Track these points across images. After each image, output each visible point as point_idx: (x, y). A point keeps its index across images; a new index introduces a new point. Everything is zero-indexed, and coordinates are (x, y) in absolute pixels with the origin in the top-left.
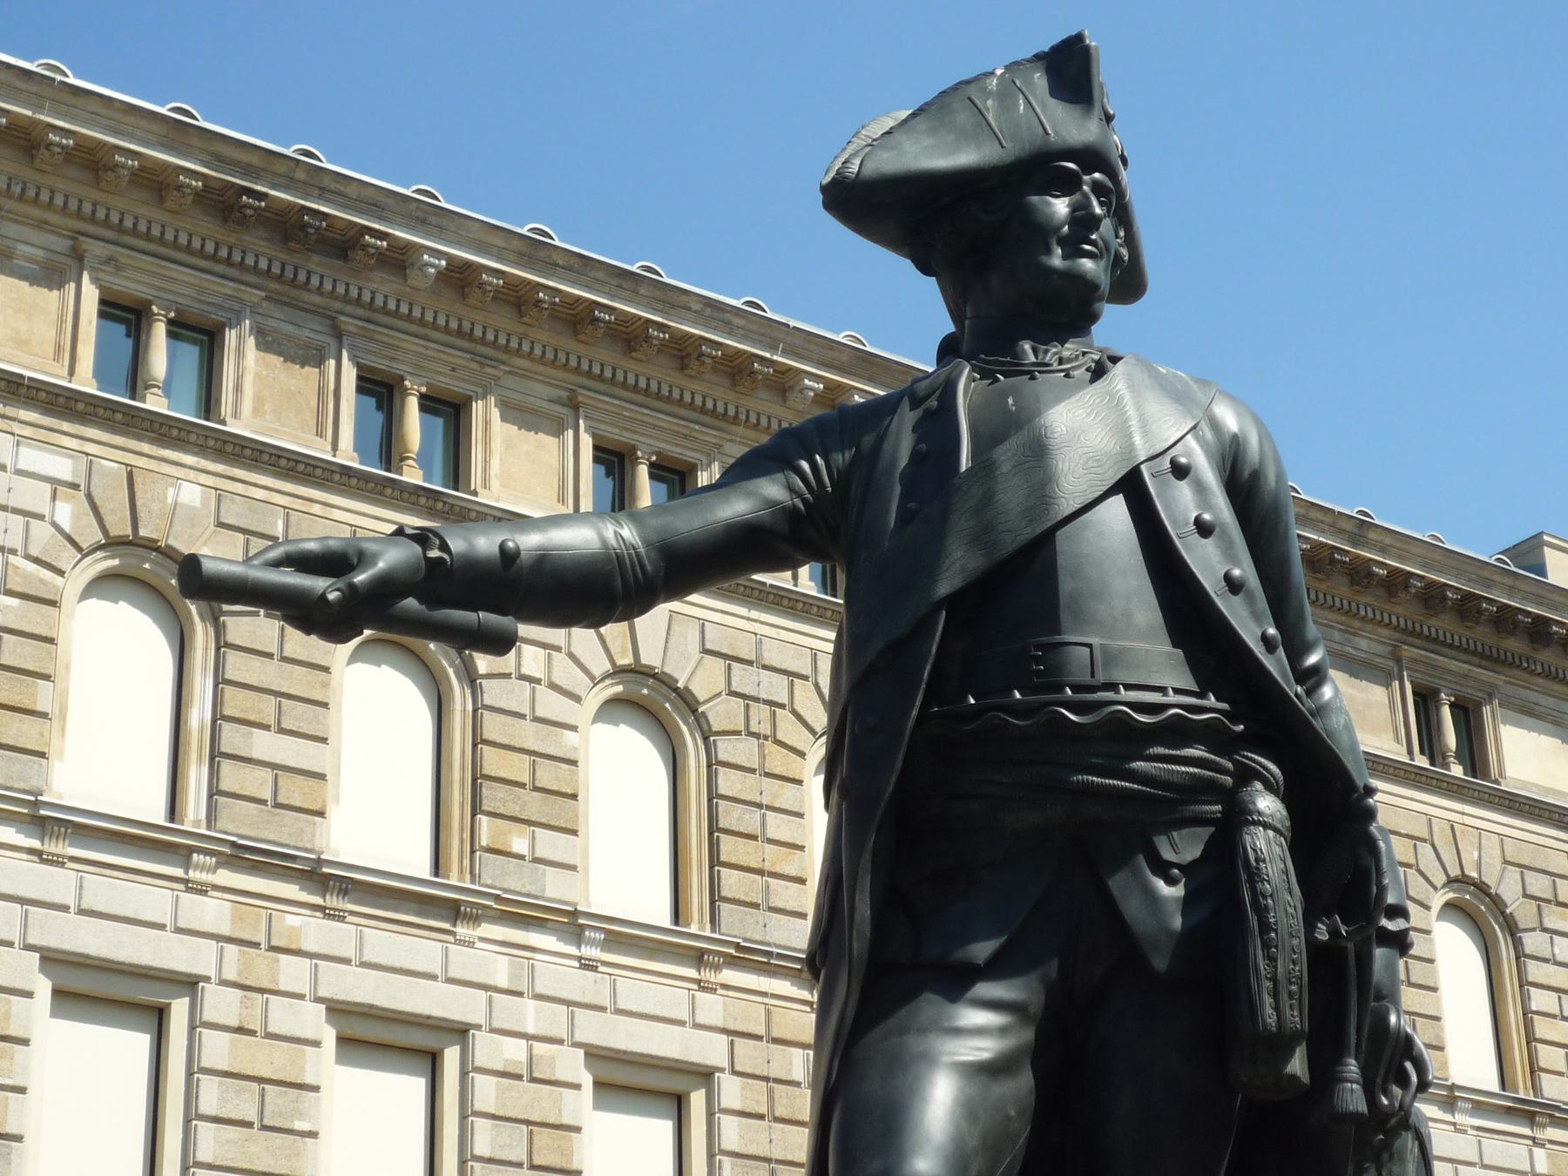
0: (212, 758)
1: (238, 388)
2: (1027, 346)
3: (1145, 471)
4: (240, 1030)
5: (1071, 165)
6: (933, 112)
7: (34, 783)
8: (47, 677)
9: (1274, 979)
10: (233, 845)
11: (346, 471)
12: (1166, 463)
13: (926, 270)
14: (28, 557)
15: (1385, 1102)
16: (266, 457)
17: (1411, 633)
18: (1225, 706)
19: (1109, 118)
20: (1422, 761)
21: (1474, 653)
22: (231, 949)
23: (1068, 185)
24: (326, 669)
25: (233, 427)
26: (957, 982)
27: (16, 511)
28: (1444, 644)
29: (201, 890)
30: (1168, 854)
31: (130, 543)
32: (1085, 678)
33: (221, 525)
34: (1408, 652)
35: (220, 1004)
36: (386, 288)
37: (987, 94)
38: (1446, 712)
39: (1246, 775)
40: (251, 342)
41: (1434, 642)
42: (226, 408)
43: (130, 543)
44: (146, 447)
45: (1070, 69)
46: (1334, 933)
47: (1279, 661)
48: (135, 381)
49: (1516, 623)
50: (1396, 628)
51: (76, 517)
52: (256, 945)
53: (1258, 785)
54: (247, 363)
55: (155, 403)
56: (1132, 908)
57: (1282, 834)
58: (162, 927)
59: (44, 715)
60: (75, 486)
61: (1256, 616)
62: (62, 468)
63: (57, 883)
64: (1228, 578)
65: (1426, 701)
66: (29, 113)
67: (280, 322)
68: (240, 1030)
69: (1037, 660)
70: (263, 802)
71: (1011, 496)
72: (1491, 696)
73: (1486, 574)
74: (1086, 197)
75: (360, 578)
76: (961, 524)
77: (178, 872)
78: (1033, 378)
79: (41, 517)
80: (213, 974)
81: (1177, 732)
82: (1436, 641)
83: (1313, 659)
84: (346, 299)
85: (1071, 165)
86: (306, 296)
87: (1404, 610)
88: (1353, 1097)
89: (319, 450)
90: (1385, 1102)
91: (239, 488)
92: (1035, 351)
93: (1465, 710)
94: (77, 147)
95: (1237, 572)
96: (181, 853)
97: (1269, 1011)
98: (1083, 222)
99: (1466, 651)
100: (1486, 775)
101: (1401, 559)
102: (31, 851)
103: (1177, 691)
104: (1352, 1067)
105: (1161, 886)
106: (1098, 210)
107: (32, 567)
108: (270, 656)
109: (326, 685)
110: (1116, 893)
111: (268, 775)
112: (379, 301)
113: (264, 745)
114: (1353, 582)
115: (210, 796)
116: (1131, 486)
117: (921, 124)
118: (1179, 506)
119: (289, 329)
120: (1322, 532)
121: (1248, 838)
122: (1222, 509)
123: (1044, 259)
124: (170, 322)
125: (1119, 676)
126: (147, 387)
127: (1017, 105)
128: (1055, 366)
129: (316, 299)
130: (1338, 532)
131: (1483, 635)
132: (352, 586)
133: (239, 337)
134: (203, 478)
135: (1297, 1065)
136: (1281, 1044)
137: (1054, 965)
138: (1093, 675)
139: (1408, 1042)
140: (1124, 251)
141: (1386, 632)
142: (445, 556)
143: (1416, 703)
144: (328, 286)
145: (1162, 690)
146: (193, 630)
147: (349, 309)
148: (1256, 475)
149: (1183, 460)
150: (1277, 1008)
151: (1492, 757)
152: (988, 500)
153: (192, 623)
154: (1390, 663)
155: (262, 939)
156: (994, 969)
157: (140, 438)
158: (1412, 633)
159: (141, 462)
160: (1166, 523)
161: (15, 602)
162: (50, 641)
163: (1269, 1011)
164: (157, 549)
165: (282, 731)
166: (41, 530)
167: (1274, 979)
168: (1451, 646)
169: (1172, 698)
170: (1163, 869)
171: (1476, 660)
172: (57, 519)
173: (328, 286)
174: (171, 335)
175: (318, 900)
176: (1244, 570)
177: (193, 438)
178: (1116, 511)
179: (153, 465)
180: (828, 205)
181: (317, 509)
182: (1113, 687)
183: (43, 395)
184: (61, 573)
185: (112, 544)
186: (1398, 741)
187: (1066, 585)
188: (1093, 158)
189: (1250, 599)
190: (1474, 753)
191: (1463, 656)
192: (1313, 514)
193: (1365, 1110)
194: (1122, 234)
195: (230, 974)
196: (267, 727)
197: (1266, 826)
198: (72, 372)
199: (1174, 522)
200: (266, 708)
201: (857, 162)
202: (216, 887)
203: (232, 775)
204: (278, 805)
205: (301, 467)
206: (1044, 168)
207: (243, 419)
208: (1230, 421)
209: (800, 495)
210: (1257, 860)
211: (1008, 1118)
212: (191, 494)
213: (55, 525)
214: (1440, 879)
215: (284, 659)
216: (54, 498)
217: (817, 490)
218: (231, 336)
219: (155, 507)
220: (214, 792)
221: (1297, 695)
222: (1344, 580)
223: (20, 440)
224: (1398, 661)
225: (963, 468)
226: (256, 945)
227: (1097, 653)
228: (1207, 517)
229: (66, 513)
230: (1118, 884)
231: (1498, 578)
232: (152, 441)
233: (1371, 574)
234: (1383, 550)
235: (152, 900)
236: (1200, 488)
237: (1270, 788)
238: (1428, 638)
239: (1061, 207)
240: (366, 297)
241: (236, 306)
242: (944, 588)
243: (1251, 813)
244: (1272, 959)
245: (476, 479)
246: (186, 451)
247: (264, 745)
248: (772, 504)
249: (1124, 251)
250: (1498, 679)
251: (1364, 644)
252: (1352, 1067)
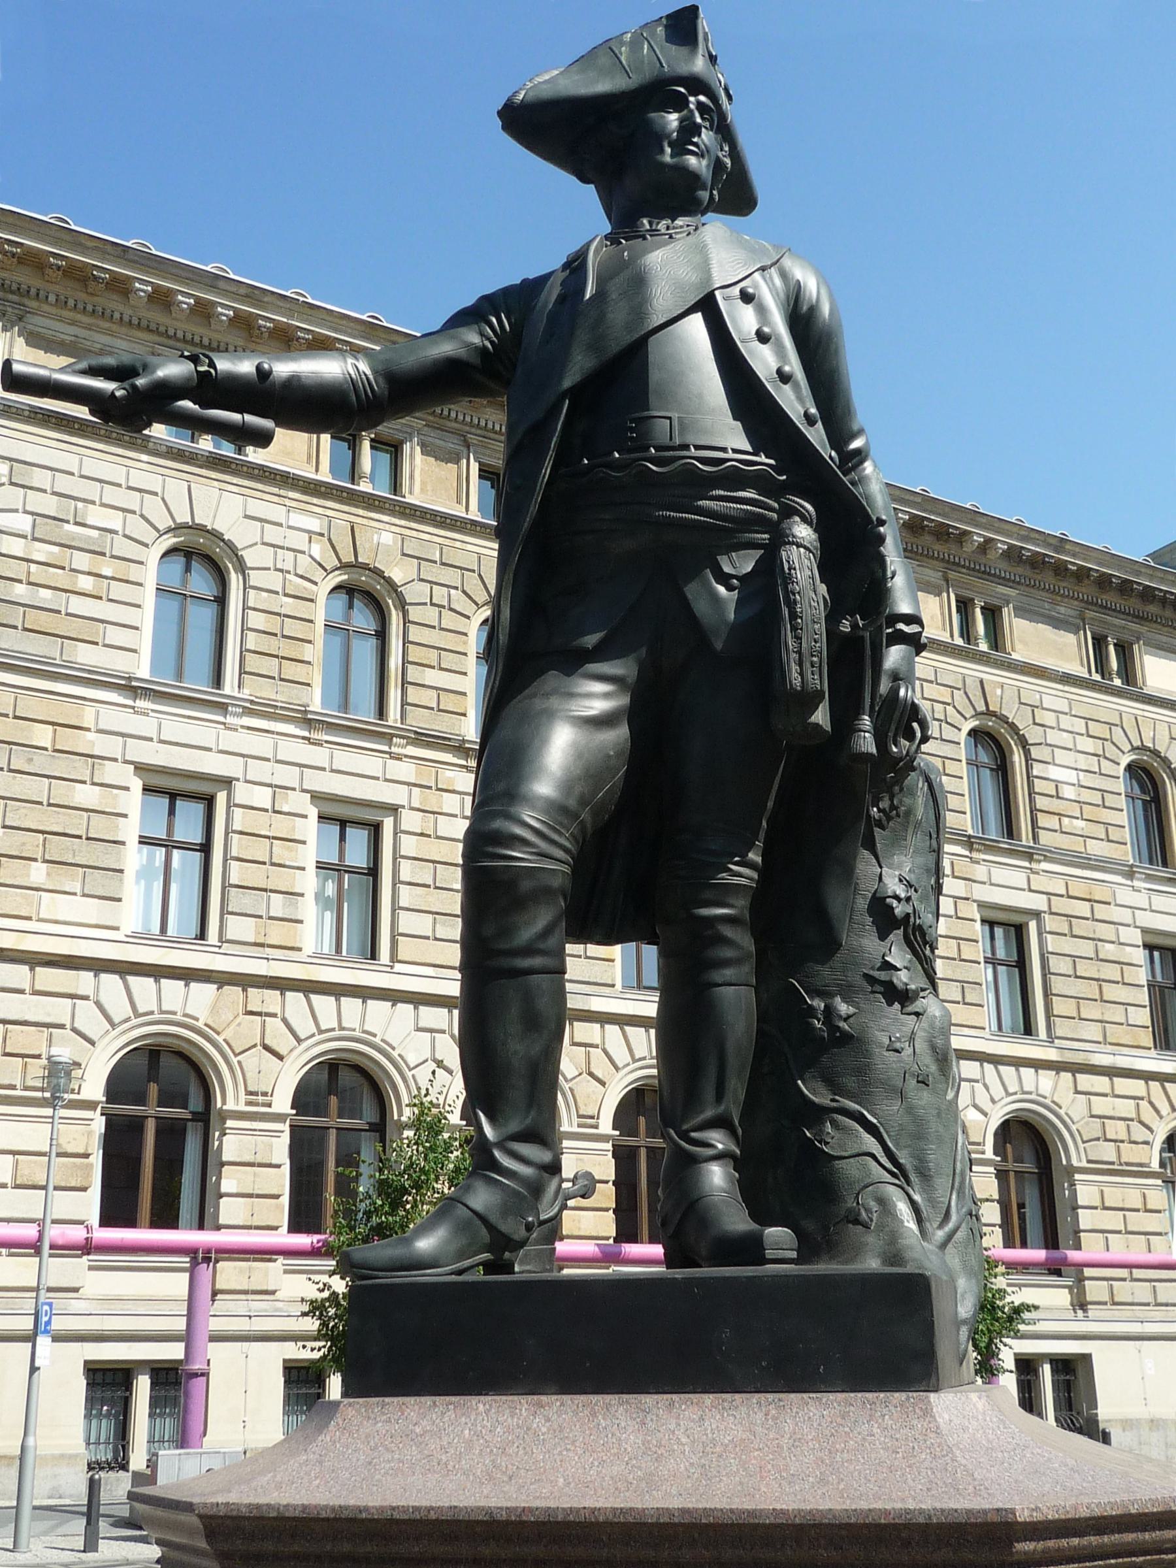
0: (403, 685)
1: (412, 477)
2: (645, 221)
3: (717, 293)
4: (422, 835)
5: (682, 90)
6: (586, 61)
7: (304, 701)
8: (310, 642)
9: (799, 653)
10: (416, 733)
11: (474, 523)
12: (736, 291)
13: (584, 179)
14: (296, 575)
15: (895, 750)
16: (418, 513)
17: (1091, 603)
18: (772, 462)
19: (713, 59)
20: (1097, 677)
21: (1129, 614)
22: (416, 790)
23: (679, 104)
24: (466, 634)
25: (409, 499)
26: (574, 661)
27: (288, 549)
28: (1110, 609)
29: (398, 758)
30: (727, 569)
31: (354, 566)
32: (665, 441)
33: (404, 555)
34: (1089, 614)
35: (410, 820)
36: (494, 418)
37: (622, 43)
38: (1111, 648)
39: (788, 512)
40: (418, 449)
41: (1104, 608)
42: (405, 489)
43: (354, 566)
44: (361, 512)
45: (682, 27)
46: (854, 626)
47: (817, 431)
48: (354, 475)
49: (1154, 596)
50: (1082, 601)
51: (323, 552)
52: (430, 788)
53: (797, 519)
54: (415, 461)
55: (365, 487)
56: (701, 607)
57: (810, 551)
58: (377, 779)
59: (309, 663)
60: (322, 535)
61: (800, 399)
62: (314, 524)
63: (318, 756)
64: (779, 372)
65: (1099, 643)
66: (285, 320)
67: (434, 438)
68: (422, 835)
69: (632, 430)
70: (432, 709)
71: (617, 315)
72: (1138, 639)
73: (1136, 567)
74: (691, 111)
75: (140, 382)
76: (582, 336)
77: (386, 748)
78: (645, 238)
79: (303, 552)
80: (406, 804)
81: (735, 478)
82: (1106, 607)
83: (856, 444)
84: (471, 424)
85: (682, 90)
86: (449, 424)
87: (1087, 590)
88: (867, 743)
89: (459, 511)
90: (895, 750)
91: (414, 534)
92: (650, 223)
93: (1123, 647)
94: (314, 339)
95: (787, 368)
96: (388, 738)
97: (795, 675)
98: (689, 129)
99: (1123, 613)
100: (1135, 685)
101: (1084, 560)
102: (304, 738)
103: (735, 451)
104: (866, 721)
105: (721, 589)
106: (699, 120)
107: (300, 580)
108: (434, 627)
109: (465, 643)
110: (689, 596)
111: (434, 693)
112: (490, 426)
113: (432, 677)
114: (1056, 575)
115: (402, 706)
116: (708, 306)
117: (574, 68)
118: (743, 321)
119: (438, 442)
120: (1038, 545)
121: (784, 553)
122: (779, 325)
123: (659, 157)
124: (372, 440)
125: (691, 439)
126: (360, 478)
127: (643, 48)
128: (663, 231)
129: (454, 425)
130: (1048, 545)
131: (1134, 603)
132: (134, 387)
133: (412, 448)
134: (393, 529)
135: (821, 716)
136: (810, 700)
137: (644, 651)
138: (671, 439)
139: (915, 708)
140: (728, 161)
141: (1076, 603)
142: (213, 371)
143: (1094, 644)
144: (461, 417)
145: (724, 450)
146: (390, 614)
147: (473, 430)
148: (813, 309)
149: (750, 290)
150: (801, 674)
151: (1139, 676)
152: (601, 318)
153: (390, 610)
154: (1078, 621)
155: (433, 785)
156: (599, 653)
157: (356, 506)
158: (1092, 603)
159: (358, 520)
160: (731, 330)
161: (291, 600)
162: (311, 621)
163: (795, 675)
164: (369, 569)
165: (441, 669)
166: (303, 560)
167: (799, 653)
168: (1114, 610)
169: (730, 455)
170: (724, 579)
171: (1130, 618)
172: (312, 553)
173: (468, 419)
174: (372, 447)
175: (463, 762)
176: (794, 366)
177: (387, 506)
178: (696, 325)
179: (365, 521)
180: (505, 128)
181: (458, 544)
182: (686, 447)
183: (301, 483)
184: (316, 583)
185: (343, 566)
186: (1082, 665)
187: (654, 376)
188: (697, 85)
189: (797, 388)
190: (1128, 672)
191: (1122, 616)
192: (1033, 535)
193: (874, 751)
194: (727, 149)
195: (415, 804)
196: (433, 667)
197: (799, 546)
198: (317, 470)
199: (739, 331)
200: (432, 656)
201: (523, 93)
202: (406, 756)
203: (413, 695)
204: (440, 710)
205: (448, 521)
206: (663, 91)
207: (414, 497)
208: (811, 285)
209: (488, 339)
210: (790, 569)
211: (609, 756)
212: (387, 538)
213: (311, 556)
214: (1127, 747)
215: (442, 629)
216: (310, 542)
217: (501, 335)
218: (407, 447)
219: (367, 546)
220: (404, 703)
221: (830, 457)
222: (1051, 573)
223: (290, 509)
224: (1083, 620)
225: (588, 296)
226: (430, 788)
227: (675, 423)
228: (766, 330)
229: (317, 550)
230: (691, 590)
231: (1143, 570)
232: (364, 508)
233: (1067, 569)
234: (1074, 555)
235: (371, 764)
236: (762, 311)
237: (804, 519)
238: (1101, 606)
239: (673, 119)
240: (483, 423)
241: (409, 430)
242: (567, 383)
243: (788, 536)
244: (798, 638)
245: (1140, 682)
246: (383, 513)
247: (432, 677)
248: (468, 345)
249: (728, 161)
250: (1144, 629)
251: (1062, 610)
252: (866, 721)
